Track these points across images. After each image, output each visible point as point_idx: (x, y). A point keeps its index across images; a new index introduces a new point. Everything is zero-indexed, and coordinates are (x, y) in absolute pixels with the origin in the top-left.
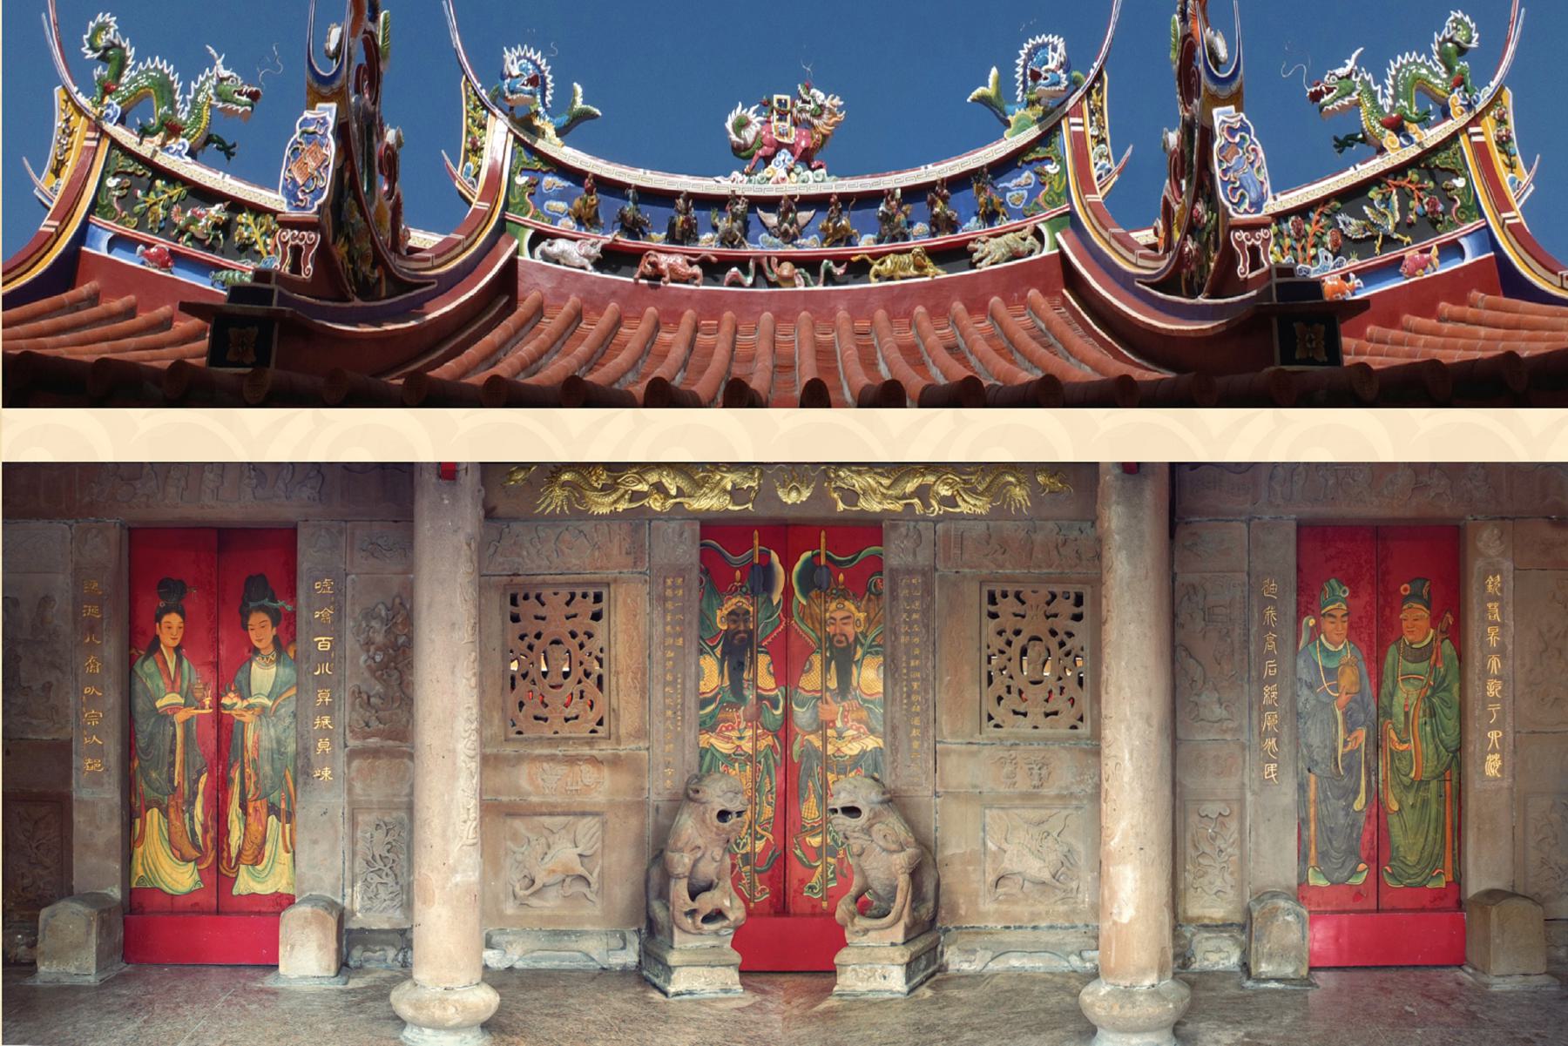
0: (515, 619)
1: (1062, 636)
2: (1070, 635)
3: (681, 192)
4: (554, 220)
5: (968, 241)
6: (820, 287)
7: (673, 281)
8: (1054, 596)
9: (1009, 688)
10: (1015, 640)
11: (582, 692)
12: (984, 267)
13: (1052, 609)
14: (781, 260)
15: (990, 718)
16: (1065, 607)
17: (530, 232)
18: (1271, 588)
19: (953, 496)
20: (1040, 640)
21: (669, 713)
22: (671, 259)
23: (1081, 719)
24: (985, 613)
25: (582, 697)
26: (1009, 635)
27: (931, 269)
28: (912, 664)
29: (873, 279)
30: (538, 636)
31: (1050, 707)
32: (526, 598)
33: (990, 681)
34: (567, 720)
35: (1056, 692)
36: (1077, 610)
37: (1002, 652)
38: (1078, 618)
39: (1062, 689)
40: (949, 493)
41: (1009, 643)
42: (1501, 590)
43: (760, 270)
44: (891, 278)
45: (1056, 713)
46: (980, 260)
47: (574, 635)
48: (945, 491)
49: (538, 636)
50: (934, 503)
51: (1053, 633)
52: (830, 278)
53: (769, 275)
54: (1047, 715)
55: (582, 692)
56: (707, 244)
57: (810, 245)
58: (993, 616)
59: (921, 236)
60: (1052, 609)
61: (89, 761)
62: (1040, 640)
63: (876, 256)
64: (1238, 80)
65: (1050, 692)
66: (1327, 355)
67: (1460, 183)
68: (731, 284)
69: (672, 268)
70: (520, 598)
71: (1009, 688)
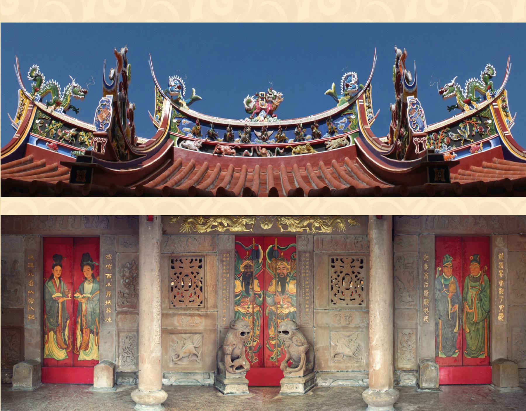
0: (173, 268)
1: (356, 274)
2: (359, 273)
3: (228, 125)
4: (186, 134)
5: (325, 141)
6: (275, 157)
7: (226, 154)
11: (195, 292)
12: (330, 150)
13: (353, 264)
14: (262, 147)
17: (178, 138)
19: (320, 227)
20: (349, 275)
21: (225, 299)
22: (225, 147)
23: (363, 301)
27: (312, 150)
29: (293, 154)
30: (181, 274)
31: (352, 297)
34: (190, 302)
35: (354, 292)
36: (361, 265)
37: (336, 279)
38: (361, 267)
39: (356, 291)
40: (318, 226)
41: (339, 276)
43: (255, 151)
44: (299, 154)
45: (354, 299)
46: (329, 147)
48: (317, 225)
49: (181, 274)
50: (313, 229)
51: (353, 273)
52: (278, 154)
53: (258, 152)
54: (351, 300)
55: (195, 292)
56: (237, 142)
57: (272, 143)
58: (333, 267)
60: (353, 264)
62: (349, 275)
63: (294, 146)
64: (415, 87)
67: (490, 121)
68: (245, 156)
69: (225, 150)
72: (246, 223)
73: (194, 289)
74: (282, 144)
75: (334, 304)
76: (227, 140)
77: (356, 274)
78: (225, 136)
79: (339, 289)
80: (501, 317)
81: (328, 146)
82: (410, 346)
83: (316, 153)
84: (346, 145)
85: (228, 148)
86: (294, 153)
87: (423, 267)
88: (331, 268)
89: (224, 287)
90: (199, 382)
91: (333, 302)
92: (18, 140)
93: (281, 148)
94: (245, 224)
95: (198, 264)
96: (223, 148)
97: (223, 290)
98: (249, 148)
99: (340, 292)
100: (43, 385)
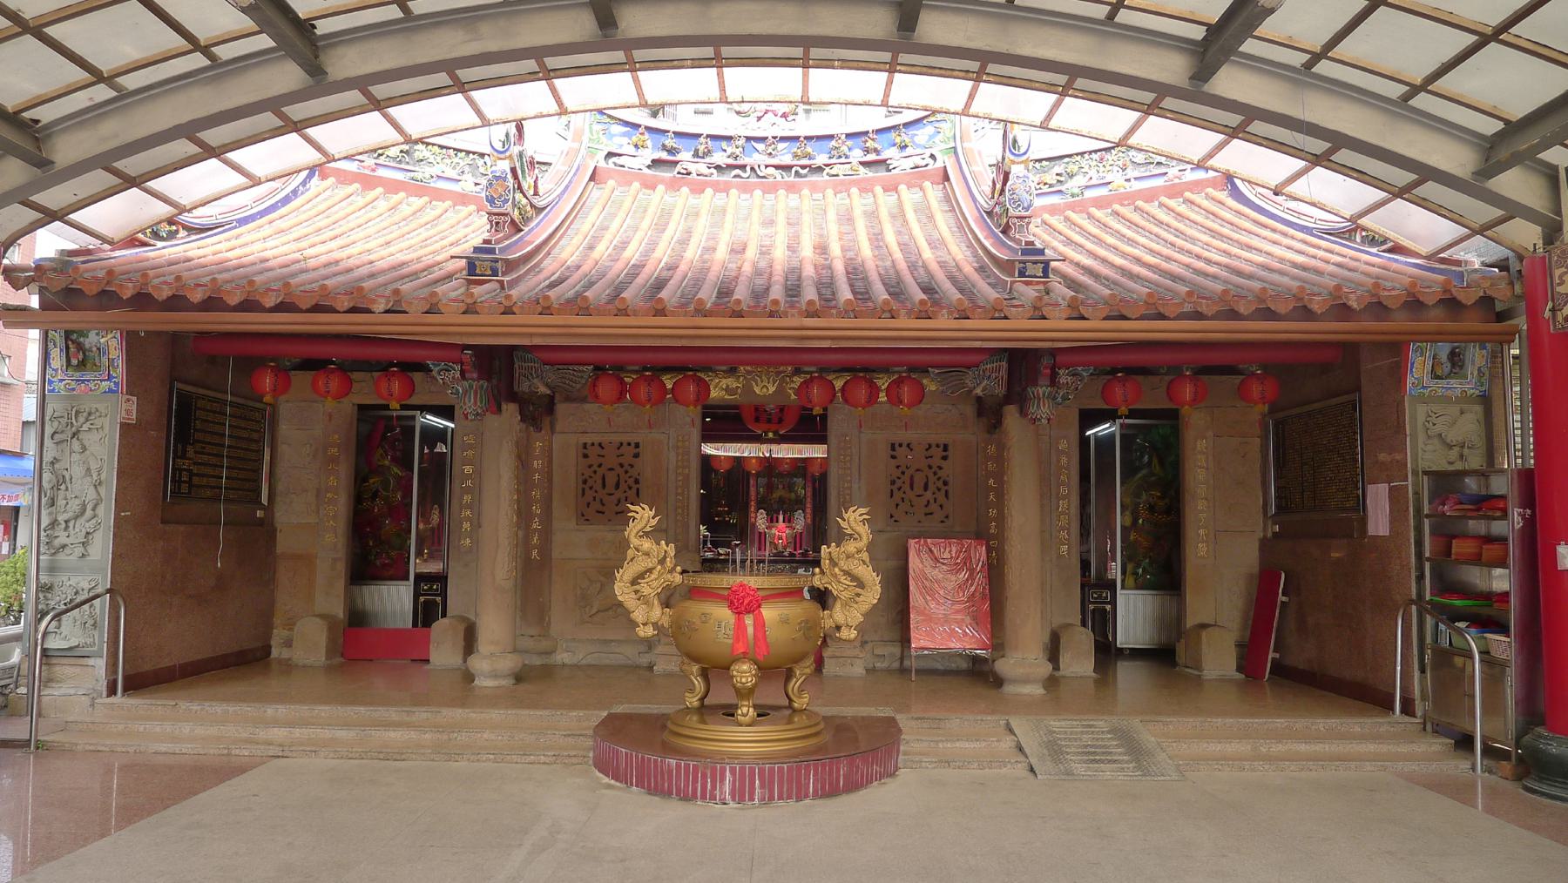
0: (585, 456)
1: (935, 468)
2: (940, 468)
5: (887, 160)
8: (930, 446)
9: (594, 498)
10: (907, 472)
11: (626, 498)
13: (929, 453)
15: (583, 515)
16: (939, 452)
18: (1063, 445)
20: (922, 471)
21: (680, 511)
23: (947, 517)
24: (580, 455)
25: (935, 502)
26: (595, 468)
28: (846, 485)
30: (600, 466)
31: (927, 510)
32: (901, 445)
33: (583, 494)
34: (617, 513)
35: (932, 501)
36: (944, 454)
37: (899, 478)
38: (945, 458)
39: (935, 499)
41: (903, 473)
42: (1206, 448)
45: (931, 514)
47: (930, 467)
49: (600, 466)
51: (930, 467)
54: (926, 514)
55: (626, 498)
56: (719, 158)
57: (787, 159)
58: (893, 457)
59: (857, 155)
60: (929, 453)
61: (328, 536)
62: (922, 471)
63: (827, 165)
65: (928, 501)
66: (1043, 272)
70: (896, 446)
71: (594, 498)
72: (728, 386)
73: (625, 492)
74: (805, 162)
75: (896, 521)
76: (700, 154)
77: (935, 468)
78: (696, 151)
79: (904, 496)
80: (1202, 549)
81: (891, 167)
82: (1049, 420)
83: (871, 174)
84: (926, 165)
85: (703, 168)
86: (827, 174)
87: (1059, 461)
88: (889, 459)
89: (680, 491)
90: (630, 659)
91: (893, 519)
92: (280, 189)
93: (803, 167)
94: (724, 387)
95: (632, 450)
96: (692, 168)
97: (677, 494)
98: (743, 167)
99: (906, 501)
100: (325, 282)
